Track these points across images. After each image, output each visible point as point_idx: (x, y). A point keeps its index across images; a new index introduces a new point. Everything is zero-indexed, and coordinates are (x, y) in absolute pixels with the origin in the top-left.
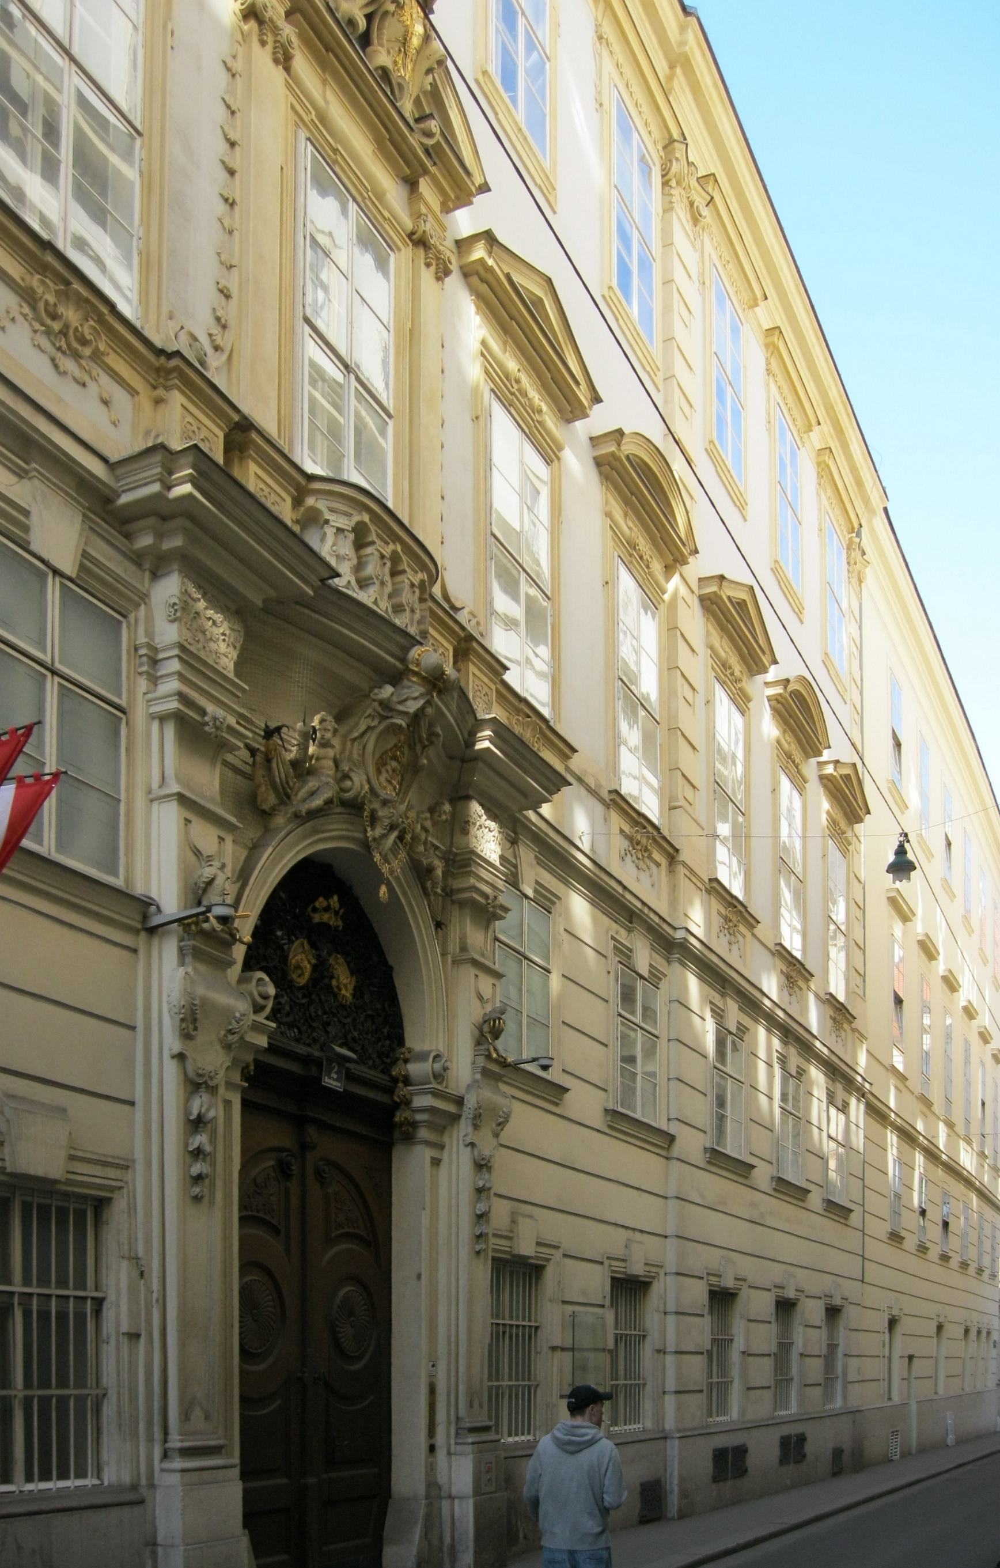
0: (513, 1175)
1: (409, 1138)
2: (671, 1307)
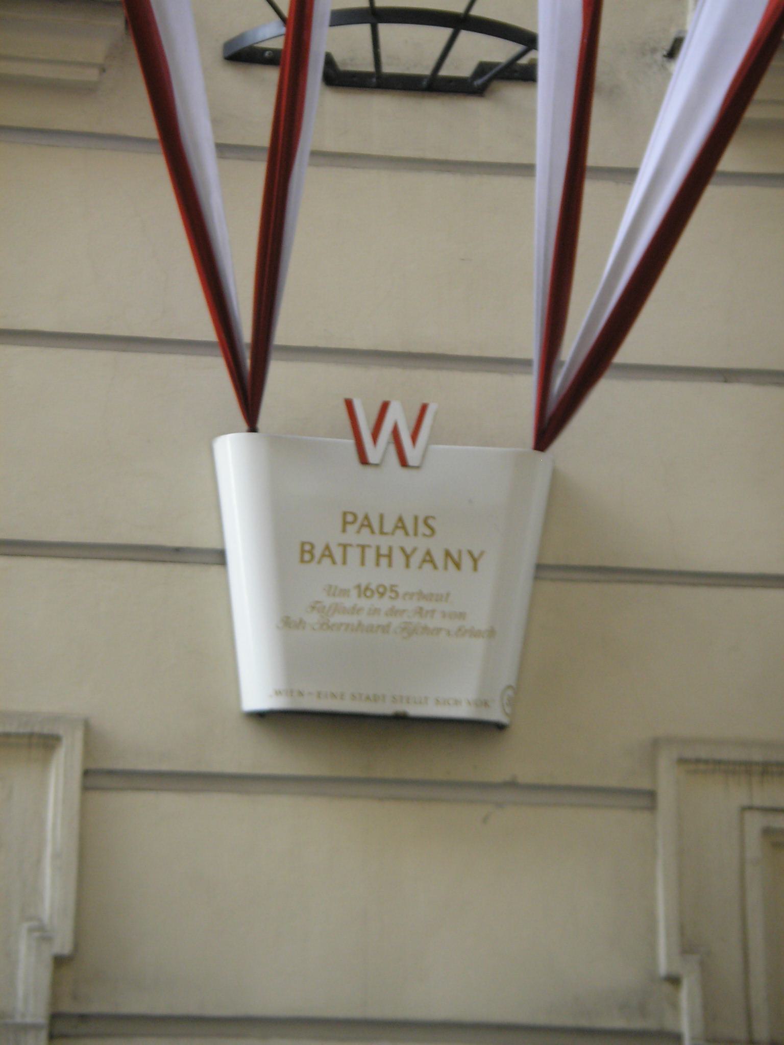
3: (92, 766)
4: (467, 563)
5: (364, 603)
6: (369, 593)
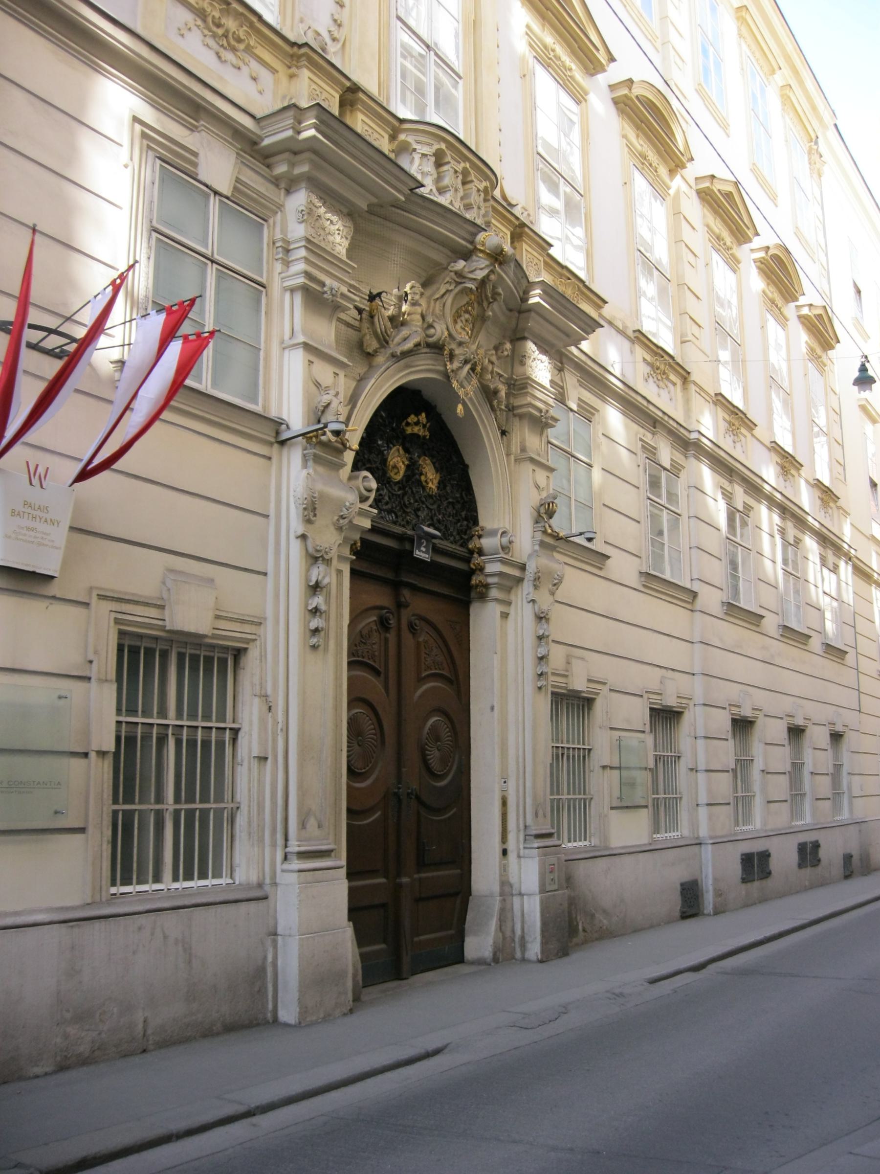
0: (566, 625)
1: (483, 597)
2: (701, 733)
4: (56, 524)
5: (27, 533)
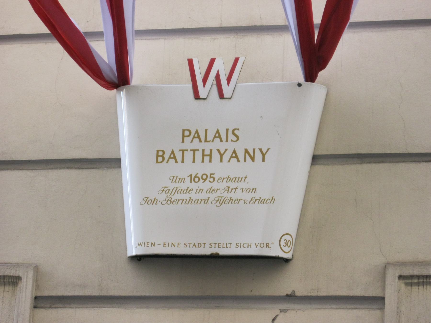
3: (39, 294)
4: (258, 156)
5: (194, 186)
6: (197, 180)
